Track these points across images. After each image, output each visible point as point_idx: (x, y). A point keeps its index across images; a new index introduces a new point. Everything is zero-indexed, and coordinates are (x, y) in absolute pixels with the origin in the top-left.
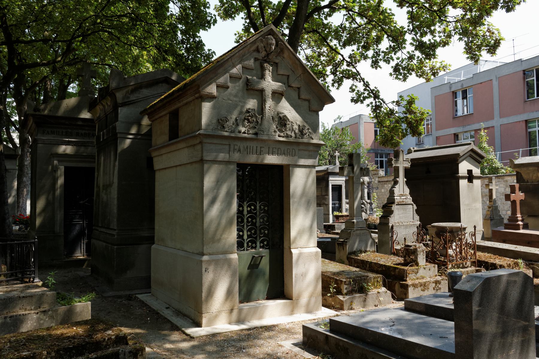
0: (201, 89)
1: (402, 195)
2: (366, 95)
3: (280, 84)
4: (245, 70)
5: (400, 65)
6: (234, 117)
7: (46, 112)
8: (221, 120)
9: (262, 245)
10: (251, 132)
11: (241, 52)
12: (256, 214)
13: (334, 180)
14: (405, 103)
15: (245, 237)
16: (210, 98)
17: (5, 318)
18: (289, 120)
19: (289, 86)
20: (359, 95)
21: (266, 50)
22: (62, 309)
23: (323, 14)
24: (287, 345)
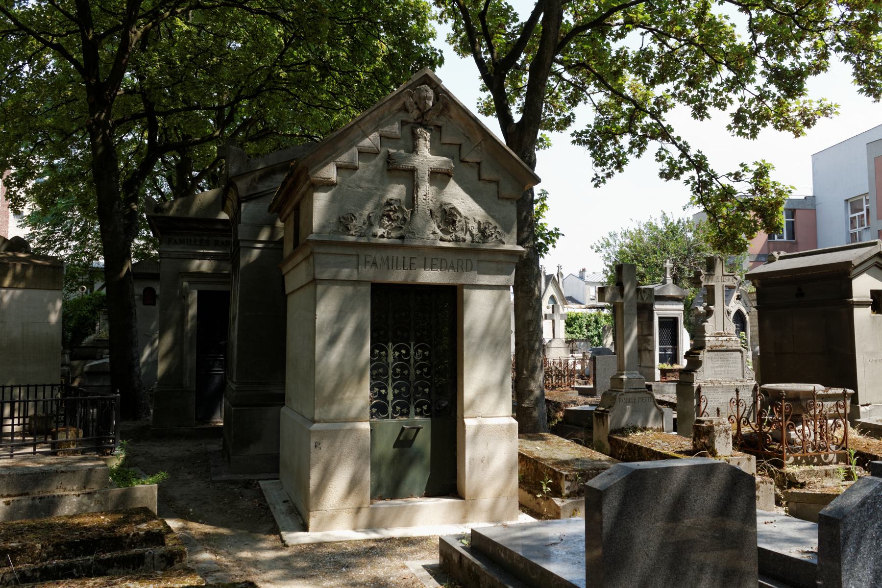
0: (310, 173)
1: (720, 335)
2: (684, 164)
3: (445, 158)
4: (384, 140)
5: (745, 111)
6: (366, 212)
7: (171, 213)
8: (344, 218)
9: (418, 410)
10: (393, 235)
11: (375, 113)
12: (408, 361)
13: (661, 310)
14: (751, 175)
15: (390, 397)
16: (327, 185)
17: (34, 499)
18: (460, 214)
19: (462, 161)
20: (672, 164)
21: (418, 108)
22: (116, 491)
23: (611, 34)
24: (416, 566)
